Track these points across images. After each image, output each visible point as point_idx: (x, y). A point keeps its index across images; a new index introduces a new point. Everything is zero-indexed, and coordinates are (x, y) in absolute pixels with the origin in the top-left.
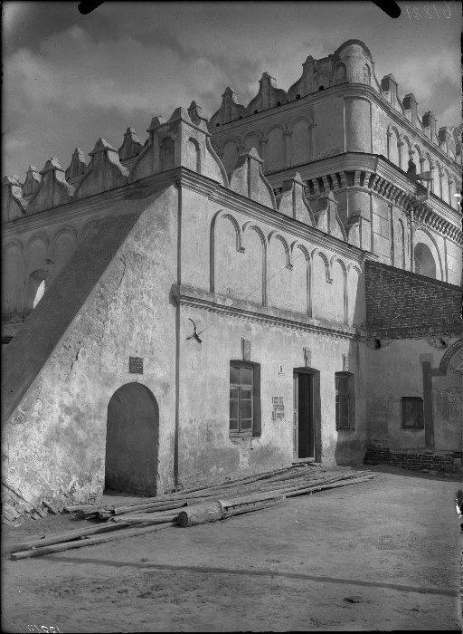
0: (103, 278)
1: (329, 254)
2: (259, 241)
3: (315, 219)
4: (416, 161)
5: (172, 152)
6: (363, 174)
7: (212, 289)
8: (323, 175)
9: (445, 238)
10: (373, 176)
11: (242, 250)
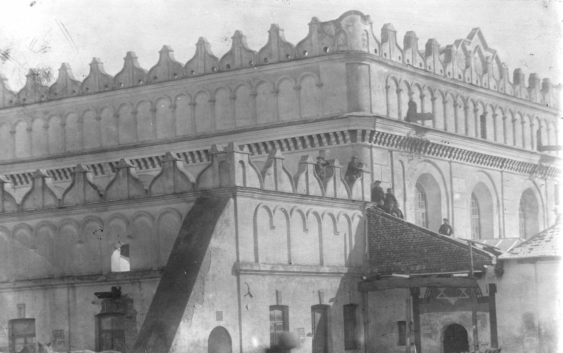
0: (202, 268)
1: (335, 211)
2: (332, 222)
3: (350, 193)
4: (418, 101)
5: (228, 171)
6: (364, 132)
7: (257, 260)
8: (330, 131)
9: (450, 162)
10: (373, 132)
11: (273, 227)
